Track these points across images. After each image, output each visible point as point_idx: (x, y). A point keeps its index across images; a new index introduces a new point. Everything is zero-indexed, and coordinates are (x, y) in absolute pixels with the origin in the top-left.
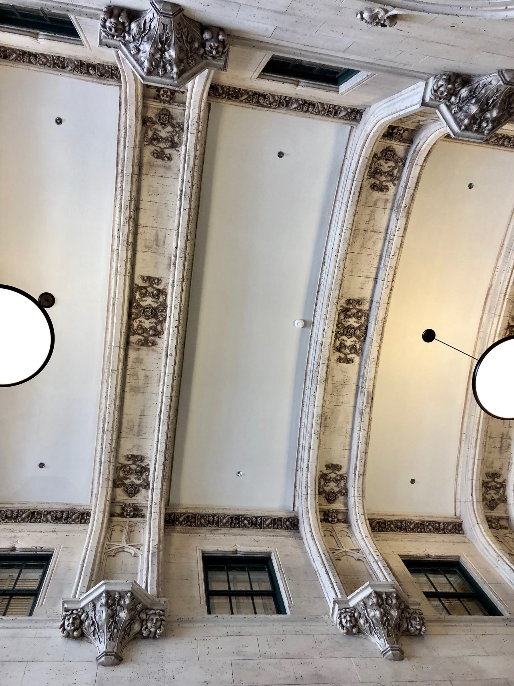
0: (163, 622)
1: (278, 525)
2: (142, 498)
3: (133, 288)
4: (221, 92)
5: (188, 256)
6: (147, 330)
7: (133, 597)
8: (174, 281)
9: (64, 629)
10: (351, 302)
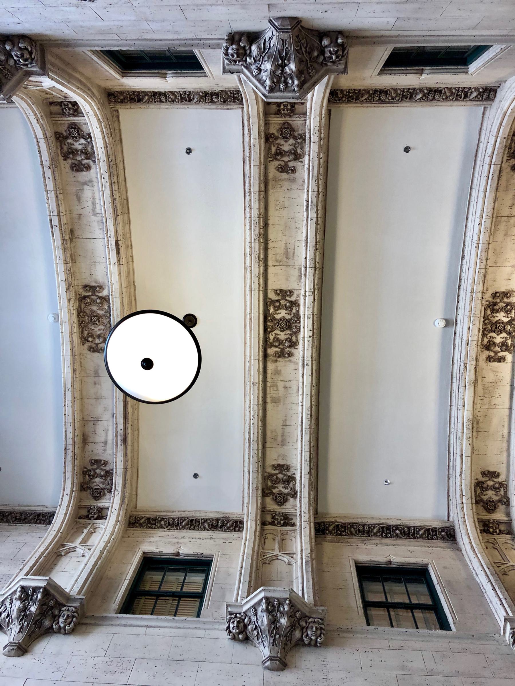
0: (323, 631)
1: (433, 536)
2: (291, 507)
3: (267, 303)
4: (341, 96)
5: (318, 266)
6: (283, 342)
7: (291, 605)
8: (305, 291)
9: (230, 632)
10: (498, 295)
